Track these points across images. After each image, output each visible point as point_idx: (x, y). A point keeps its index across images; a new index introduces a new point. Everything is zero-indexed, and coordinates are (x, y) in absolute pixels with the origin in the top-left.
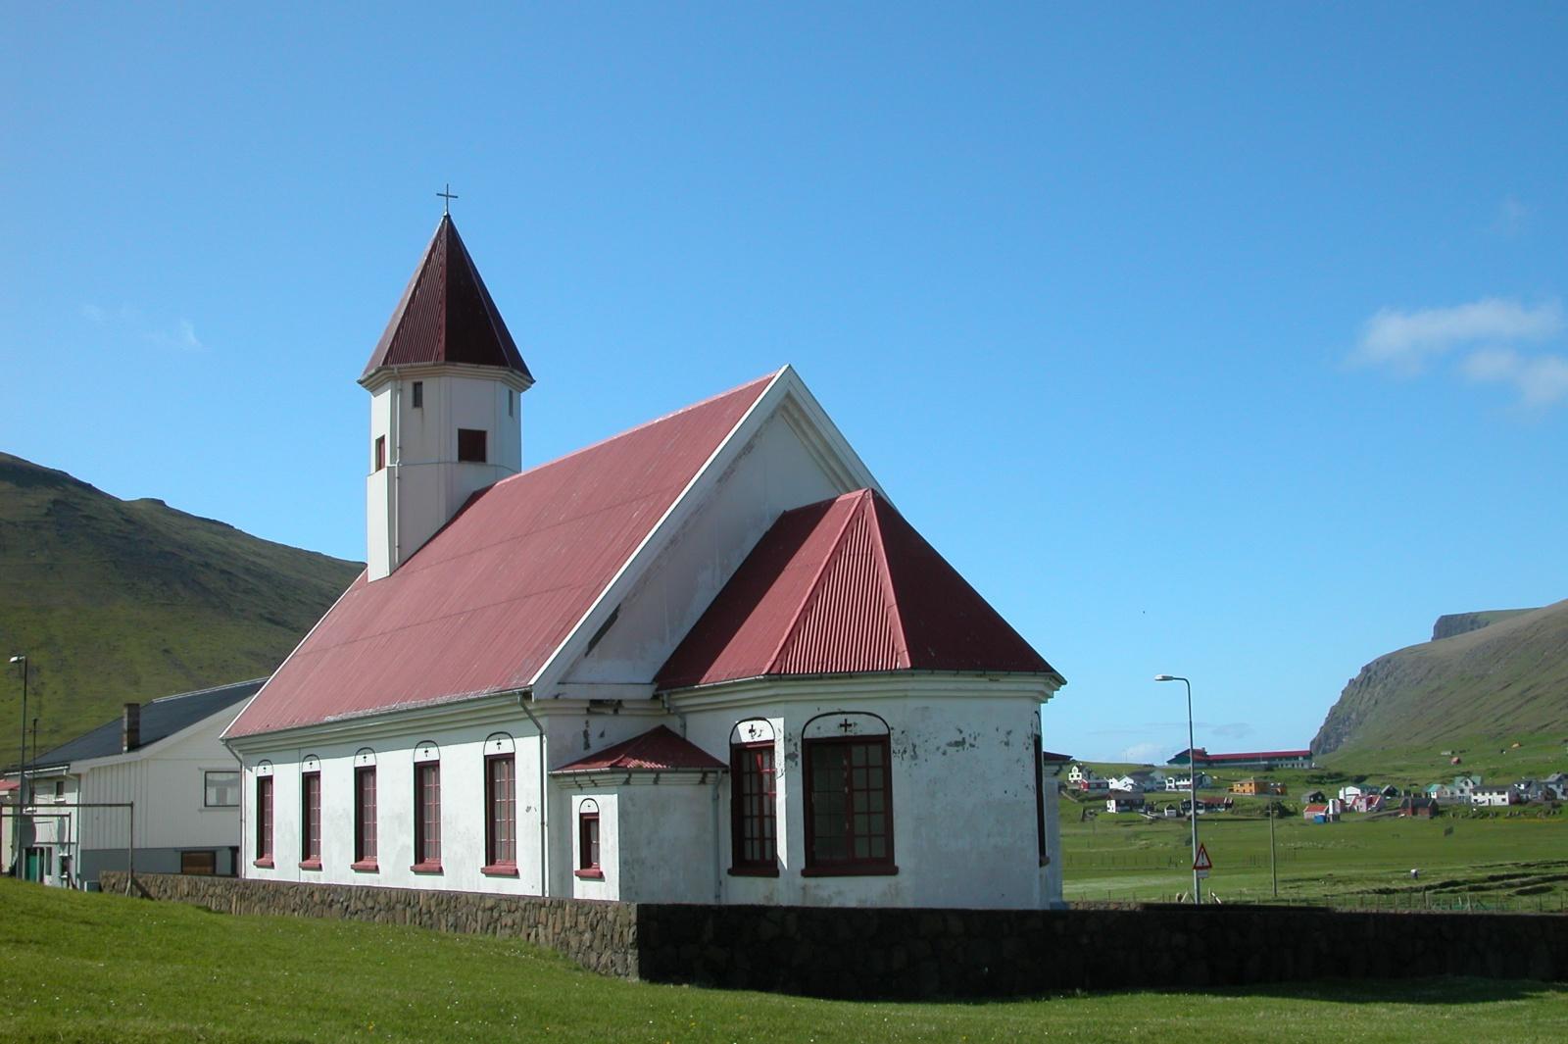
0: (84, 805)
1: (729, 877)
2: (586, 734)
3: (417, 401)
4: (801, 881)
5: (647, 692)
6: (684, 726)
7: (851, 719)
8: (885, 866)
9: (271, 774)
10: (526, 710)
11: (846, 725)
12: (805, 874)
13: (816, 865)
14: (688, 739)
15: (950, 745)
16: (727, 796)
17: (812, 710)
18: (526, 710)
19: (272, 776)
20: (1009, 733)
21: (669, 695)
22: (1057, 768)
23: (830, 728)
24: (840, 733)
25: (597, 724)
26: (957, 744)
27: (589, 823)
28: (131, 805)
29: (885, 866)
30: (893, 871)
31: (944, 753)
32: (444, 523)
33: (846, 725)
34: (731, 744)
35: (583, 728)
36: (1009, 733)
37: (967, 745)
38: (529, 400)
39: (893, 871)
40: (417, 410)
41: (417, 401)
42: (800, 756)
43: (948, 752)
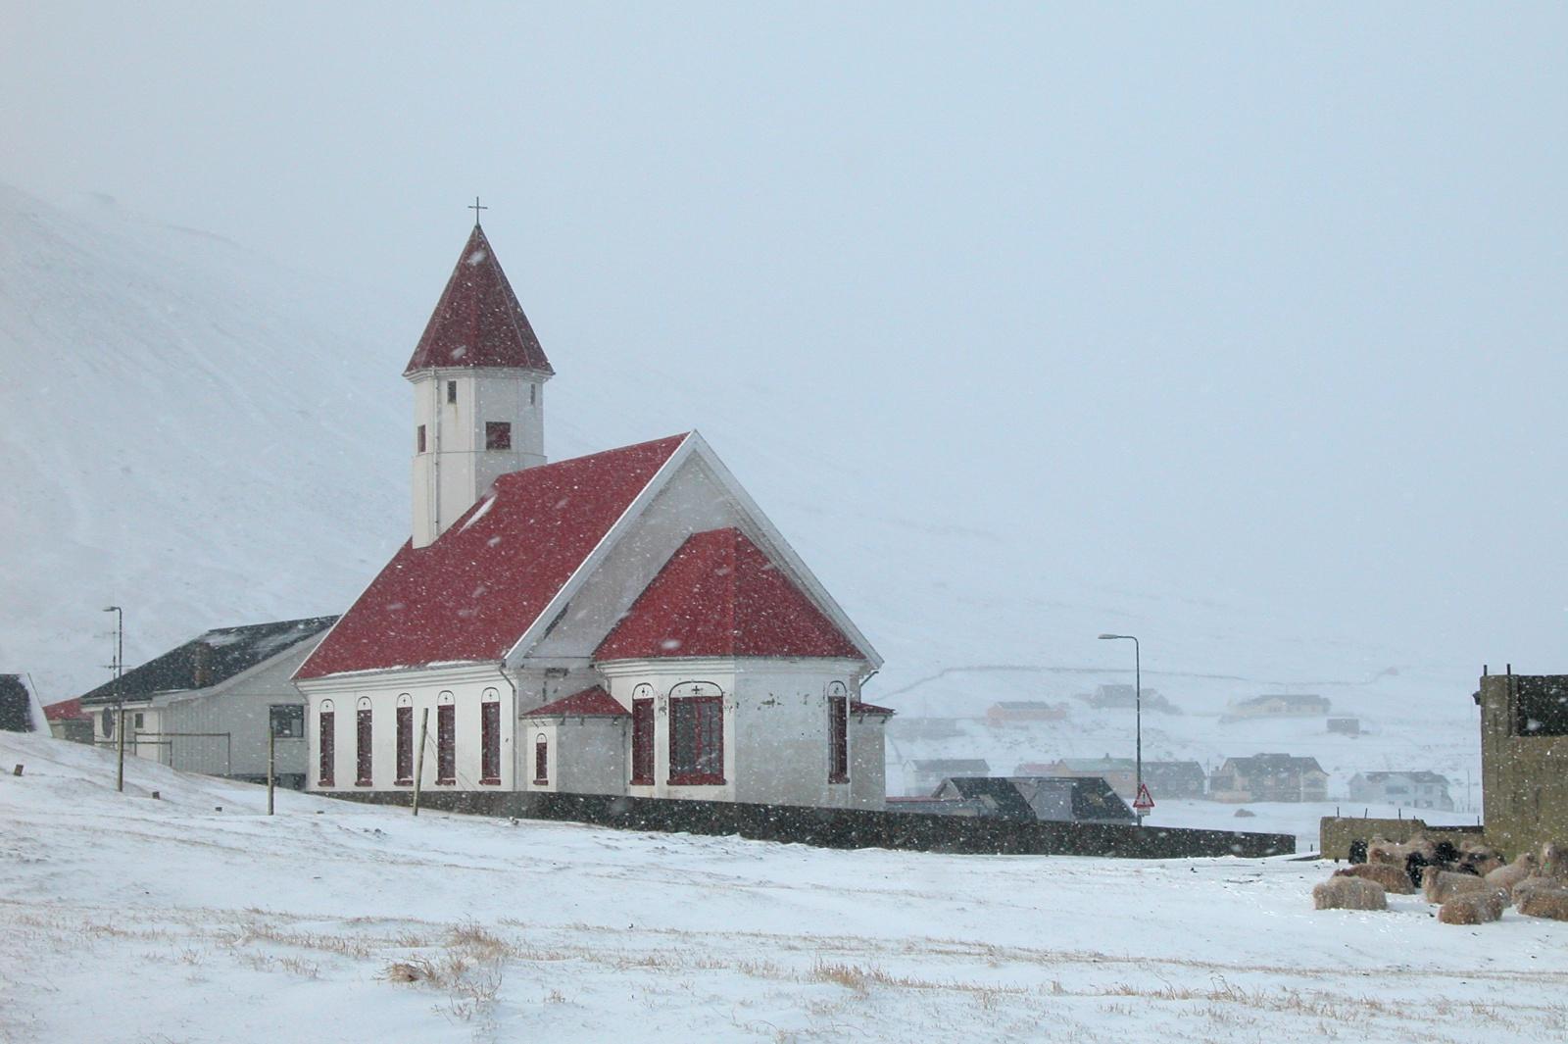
0: (162, 743)
1: (632, 787)
2: (544, 691)
3: (452, 397)
4: (667, 787)
5: (586, 663)
6: (609, 687)
7: (700, 686)
8: (718, 779)
9: (497, 700)
10: (502, 673)
11: (696, 690)
12: (669, 783)
13: (676, 779)
14: (613, 695)
15: (764, 703)
16: (631, 733)
17: (673, 680)
18: (502, 673)
19: (453, 706)
20: (807, 696)
21: (600, 665)
22: (883, 718)
23: (686, 692)
24: (693, 694)
25: (552, 684)
26: (768, 703)
27: (542, 750)
28: (229, 735)
29: (718, 779)
30: (724, 782)
31: (759, 709)
32: (473, 503)
33: (696, 690)
34: (634, 700)
35: (543, 686)
36: (807, 696)
37: (776, 703)
38: (550, 389)
39: (724, 782)
40: (451, 407)
41: (452, 397)
42: (668, 708)
43: (762, 709)
